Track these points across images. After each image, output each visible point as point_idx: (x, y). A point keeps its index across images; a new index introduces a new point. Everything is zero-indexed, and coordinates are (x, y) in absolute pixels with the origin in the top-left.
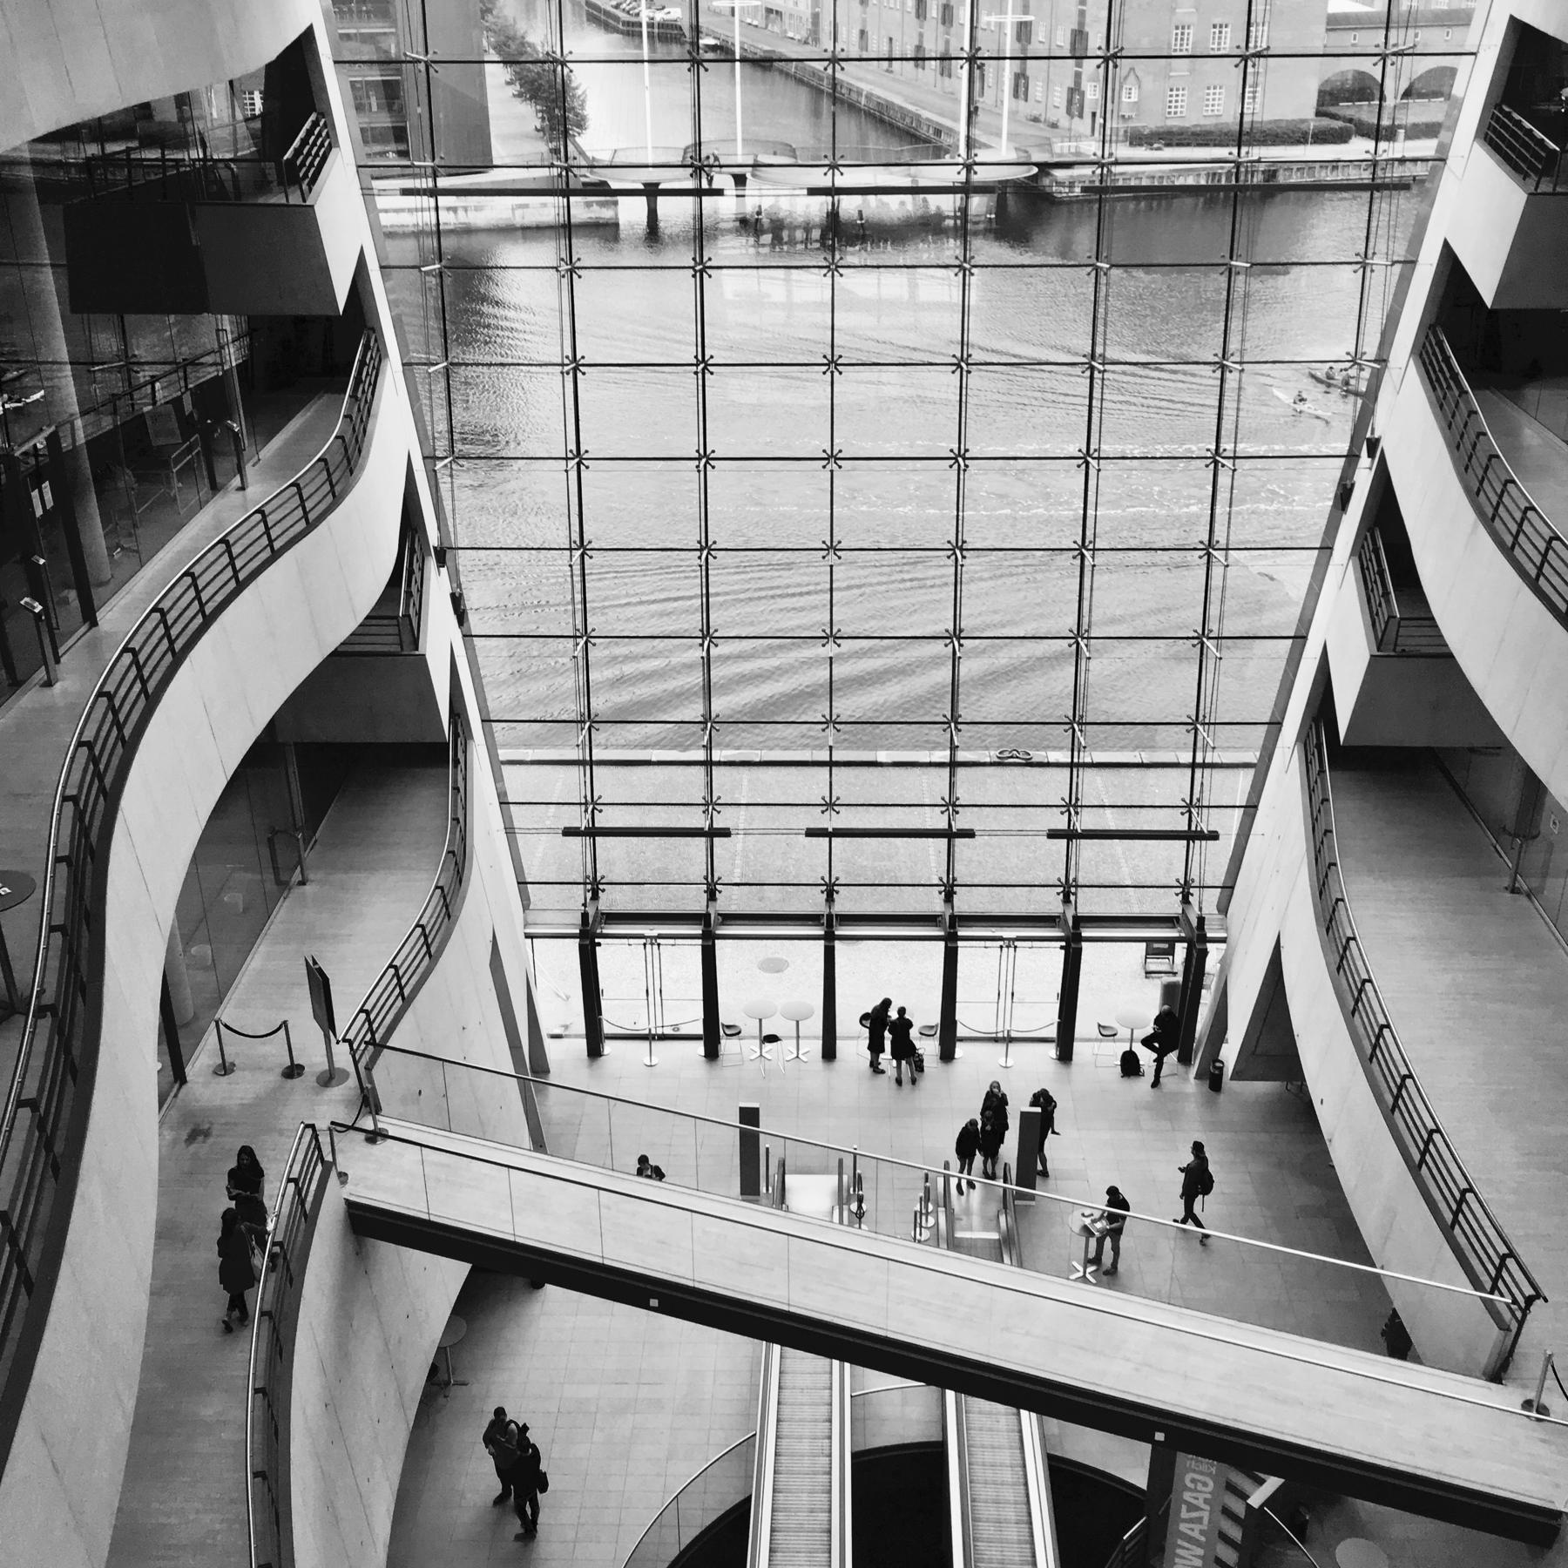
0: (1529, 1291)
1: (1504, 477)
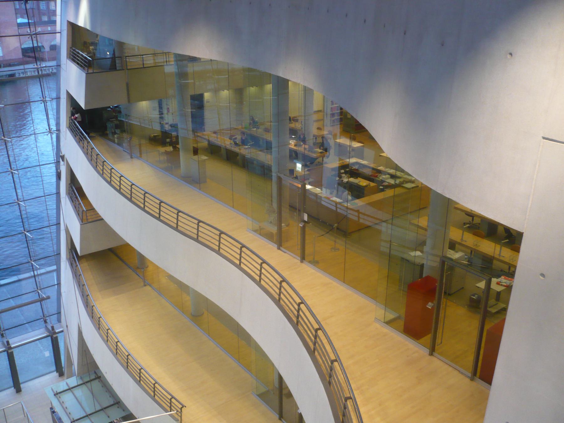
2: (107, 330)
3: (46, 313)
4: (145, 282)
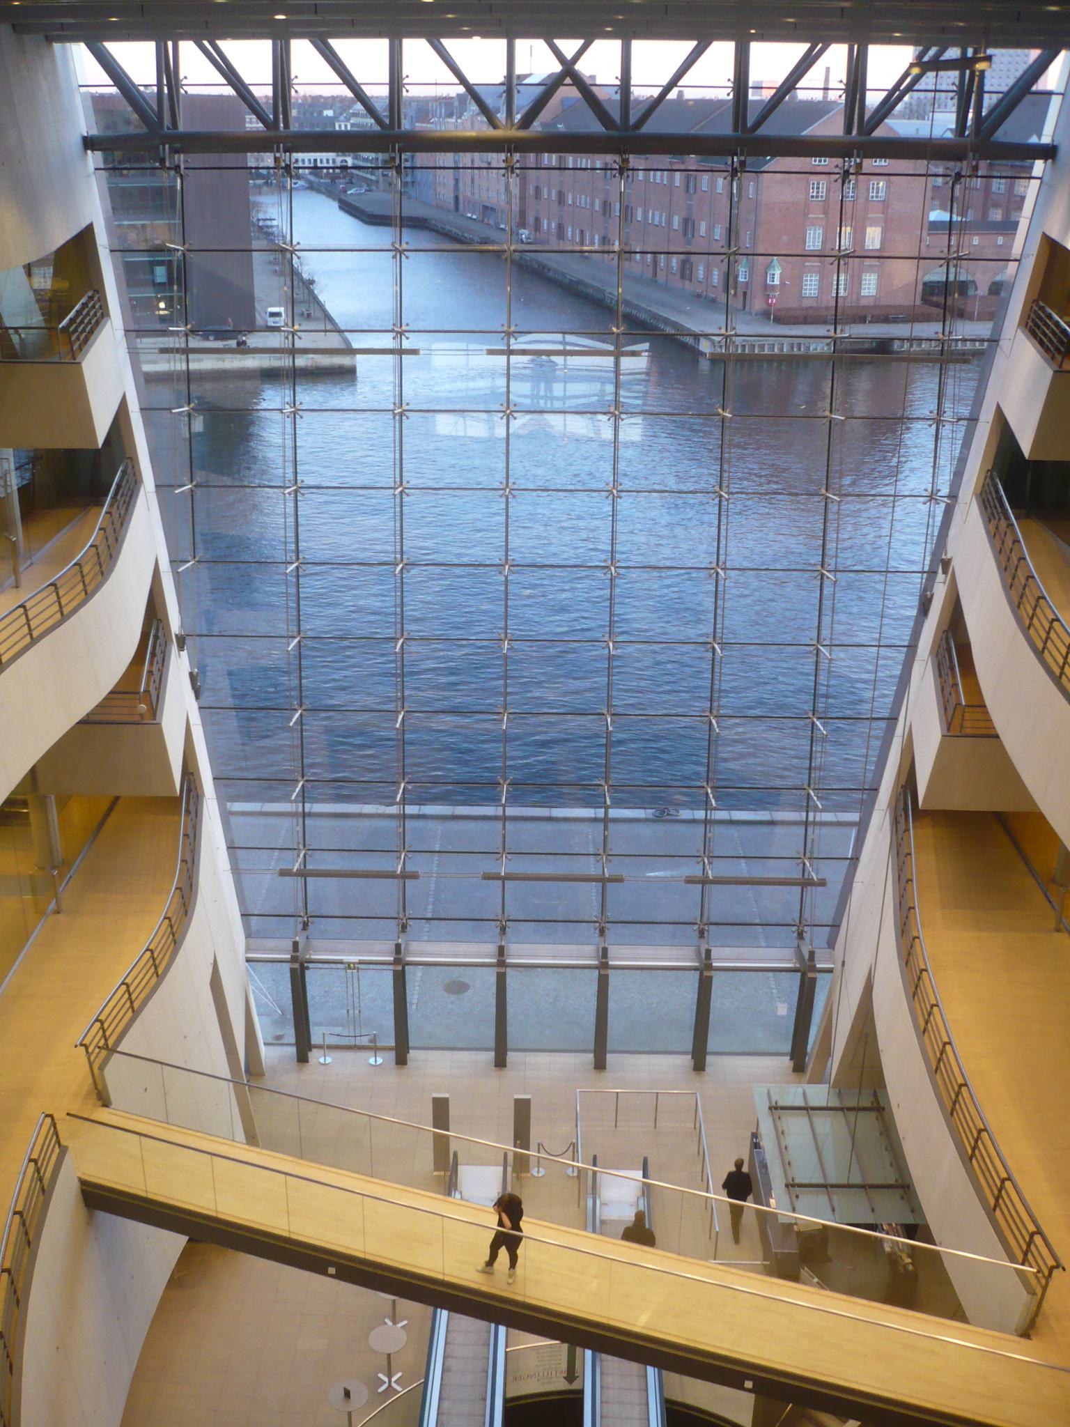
0: (1051, 1262)
1: (1037, 594)
2: (932, 1006)
3: (807, 915)
4: (1059, 920)
